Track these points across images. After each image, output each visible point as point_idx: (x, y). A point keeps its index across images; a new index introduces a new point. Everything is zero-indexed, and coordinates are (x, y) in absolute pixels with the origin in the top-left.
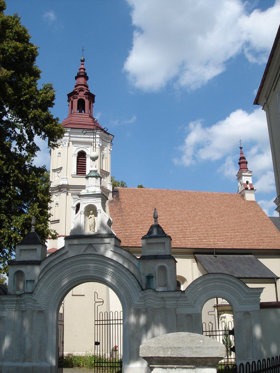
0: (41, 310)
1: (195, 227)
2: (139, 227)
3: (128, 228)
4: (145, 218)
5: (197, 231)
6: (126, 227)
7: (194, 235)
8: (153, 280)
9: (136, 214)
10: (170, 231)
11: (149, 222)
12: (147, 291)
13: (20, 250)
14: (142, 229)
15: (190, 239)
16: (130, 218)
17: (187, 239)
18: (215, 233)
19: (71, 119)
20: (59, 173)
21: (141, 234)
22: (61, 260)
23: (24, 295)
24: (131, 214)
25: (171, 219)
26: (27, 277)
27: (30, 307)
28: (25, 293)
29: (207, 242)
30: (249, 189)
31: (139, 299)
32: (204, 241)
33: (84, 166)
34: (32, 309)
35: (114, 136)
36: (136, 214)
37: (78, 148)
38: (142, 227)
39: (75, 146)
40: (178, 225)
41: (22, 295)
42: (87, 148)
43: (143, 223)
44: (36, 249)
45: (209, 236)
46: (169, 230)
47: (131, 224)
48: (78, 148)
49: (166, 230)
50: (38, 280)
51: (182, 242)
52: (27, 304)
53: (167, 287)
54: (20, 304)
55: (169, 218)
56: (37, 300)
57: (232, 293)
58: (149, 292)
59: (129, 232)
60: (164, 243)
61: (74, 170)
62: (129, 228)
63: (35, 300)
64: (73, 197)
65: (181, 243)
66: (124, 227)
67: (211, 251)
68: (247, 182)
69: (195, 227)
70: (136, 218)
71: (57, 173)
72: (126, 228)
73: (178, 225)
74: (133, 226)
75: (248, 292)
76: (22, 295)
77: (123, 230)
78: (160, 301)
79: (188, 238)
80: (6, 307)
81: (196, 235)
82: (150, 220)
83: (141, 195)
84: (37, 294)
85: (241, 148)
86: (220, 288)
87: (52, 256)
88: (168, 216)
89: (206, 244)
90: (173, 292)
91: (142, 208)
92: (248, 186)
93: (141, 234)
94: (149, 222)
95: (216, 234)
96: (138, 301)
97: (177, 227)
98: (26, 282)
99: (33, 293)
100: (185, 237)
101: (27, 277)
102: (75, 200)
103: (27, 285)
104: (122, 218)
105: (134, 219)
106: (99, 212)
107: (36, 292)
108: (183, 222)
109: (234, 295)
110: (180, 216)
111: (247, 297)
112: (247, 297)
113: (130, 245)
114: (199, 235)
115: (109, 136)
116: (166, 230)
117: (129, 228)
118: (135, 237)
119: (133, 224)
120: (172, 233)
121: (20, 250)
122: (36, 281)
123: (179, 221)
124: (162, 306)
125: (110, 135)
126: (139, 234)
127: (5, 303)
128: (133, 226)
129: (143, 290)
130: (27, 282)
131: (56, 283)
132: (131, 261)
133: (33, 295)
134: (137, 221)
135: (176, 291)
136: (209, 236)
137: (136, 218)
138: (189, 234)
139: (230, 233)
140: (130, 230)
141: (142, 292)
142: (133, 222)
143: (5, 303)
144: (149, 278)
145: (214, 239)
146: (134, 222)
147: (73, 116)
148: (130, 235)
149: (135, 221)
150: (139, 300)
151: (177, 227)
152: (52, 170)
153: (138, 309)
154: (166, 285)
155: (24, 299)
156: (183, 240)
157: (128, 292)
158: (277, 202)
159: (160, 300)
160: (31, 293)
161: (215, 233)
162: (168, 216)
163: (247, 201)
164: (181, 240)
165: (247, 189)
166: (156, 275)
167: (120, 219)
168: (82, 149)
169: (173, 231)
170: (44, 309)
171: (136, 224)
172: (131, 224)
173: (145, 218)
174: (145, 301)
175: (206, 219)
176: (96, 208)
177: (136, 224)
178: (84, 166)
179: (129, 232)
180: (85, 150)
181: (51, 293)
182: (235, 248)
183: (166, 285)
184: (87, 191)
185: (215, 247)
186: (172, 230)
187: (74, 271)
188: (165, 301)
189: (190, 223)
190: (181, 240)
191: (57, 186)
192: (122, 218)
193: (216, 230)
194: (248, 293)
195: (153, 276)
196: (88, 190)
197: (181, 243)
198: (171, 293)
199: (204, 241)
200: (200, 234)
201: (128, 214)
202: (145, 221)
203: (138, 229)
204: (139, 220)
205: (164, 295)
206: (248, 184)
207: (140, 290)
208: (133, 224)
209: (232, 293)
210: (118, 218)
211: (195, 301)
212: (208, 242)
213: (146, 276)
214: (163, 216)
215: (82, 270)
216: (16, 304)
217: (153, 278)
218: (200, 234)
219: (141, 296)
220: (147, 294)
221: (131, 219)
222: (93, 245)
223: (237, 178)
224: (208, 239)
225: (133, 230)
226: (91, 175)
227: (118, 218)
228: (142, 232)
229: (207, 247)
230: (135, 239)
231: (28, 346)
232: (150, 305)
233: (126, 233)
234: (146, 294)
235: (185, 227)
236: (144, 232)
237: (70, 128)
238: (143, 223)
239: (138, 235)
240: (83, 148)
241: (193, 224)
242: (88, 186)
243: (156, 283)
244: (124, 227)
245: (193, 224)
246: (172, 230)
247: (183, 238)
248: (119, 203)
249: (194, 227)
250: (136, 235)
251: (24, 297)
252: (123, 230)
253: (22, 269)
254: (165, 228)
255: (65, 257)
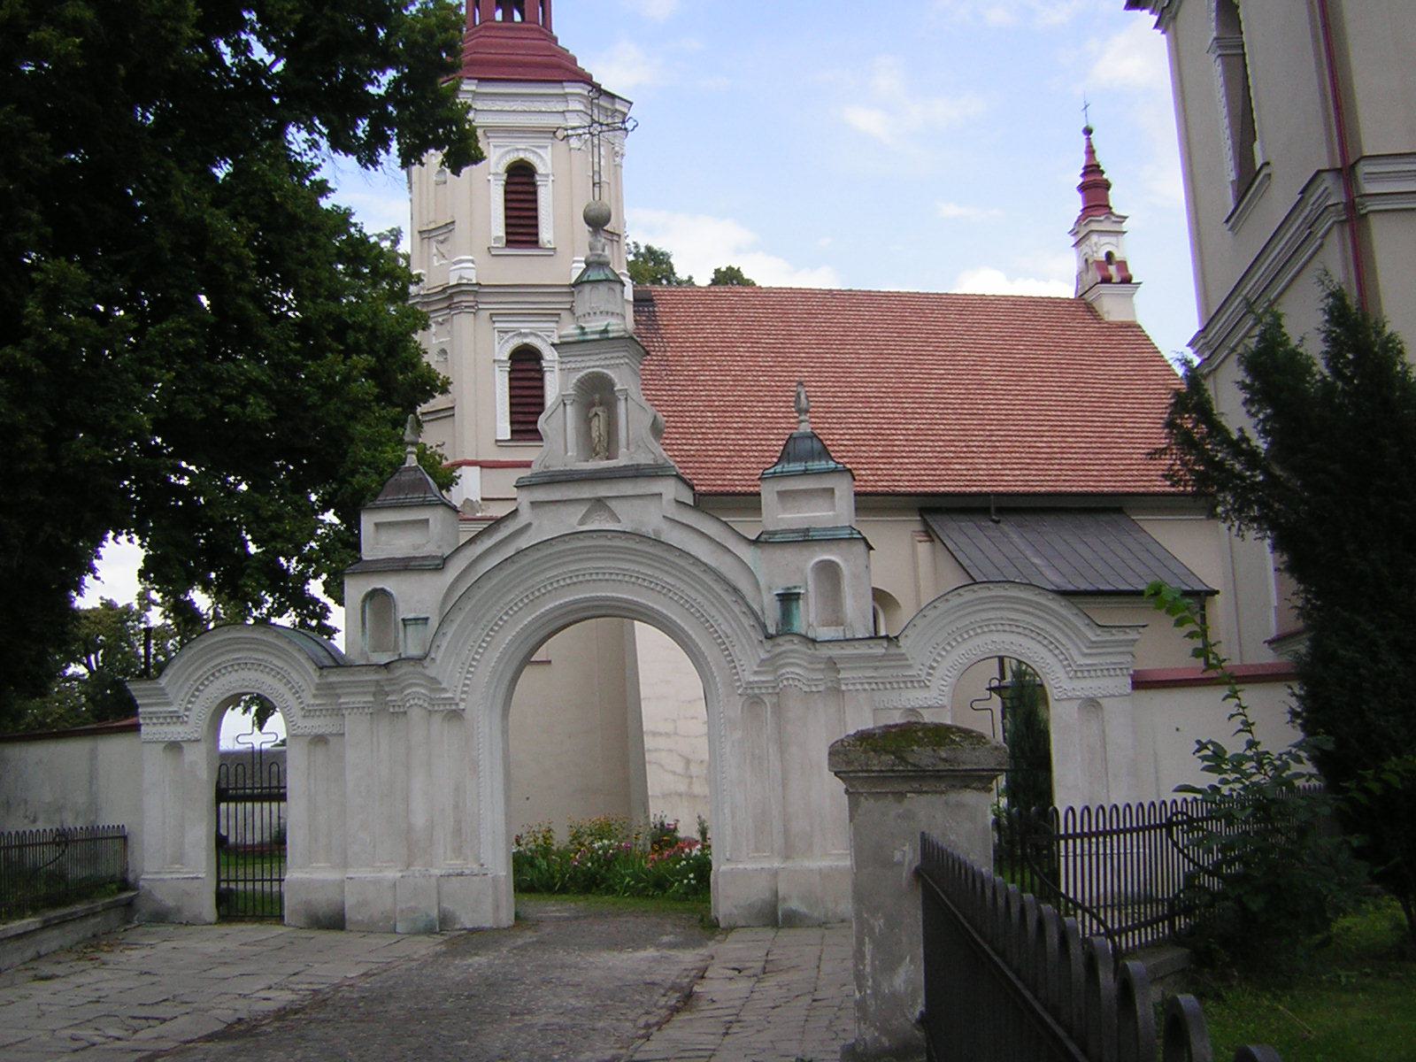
0: (454, 707)
1: (924, 421)
2: (730, 425)
3: (692, 430)
4: (751, 393)
5: (930, 432)
6: (685, 425)
7: (923, 449)
8: (798, 608)
9: (719, 378)
10: (837, 437)
11: (765, 404)
12: (780, 640)
13: (377, 525)
14: (739, 431)
15: (906, 460)
16: (697, 393)
17: (896, 460)
18: (994, 438)
19: (477, 45)
20: (442, 242)
21: (737, 448)
22: (510, 551)
23: (398, 664)
24: (702, 378)
25: (840, 394)
26: (404, 611)
27: (421, 702)
28: (400, 659)
29: (965, 472)
30: (1116, 278)
31: (317, 689)
32: (957, 467)
33: (530, 214)
34: (426, 705)
35: (631, 103)
36: (719, 378)
37: (508, 152)
38: (740, 425)
39: (495, 146)
40: (865, 415)
41: (391, 665)
42: (538, 151)
43: (745, 409)
44: (427, 521)
45: (975, 449)
46: (835, 431)
47: (704, 414)
48: (508, 152)
49: (825, 431)
50: (441, 613)
51: (879, 472)
52: (406, 692)
53: (842, 625)
54: (387, 694)
55: (833, 389)
56: (440, 678)
57: (1045, 642)
58: (785, 645)
59: (696, 442)
60: (832, 490)
61: (498, 227)
62: (698, 431)
63: (434, 680)
64: (497, 325)
65: (876, 478)
66: (679, 425)
67: (977, 503)
68: (1109, 255)
69: (924, 421)
70: (719, 393)
71: (438, 242)
72: (686, 430)
73: (865, 415)
74: (711, 420)
75: (1094, 639)
76: (395, 664)
77: (677, 436)
78: (822, 670)
79: (901, 460)
80: (343, 703)
81: (928, 449)
82: (766, 399)
83: (732, 309)
84: (438, 662)
85: (1088, 131)
86: (1007, 628)
87: (478, 542)
88: (830, 384)
89: (963, 478)
90: (863, 642)
91: (739, 359)
92: (1112, 269)
93: (737, 448)
94: (765, 404)
95: (998, 444)
96: (756, 673)
97: (862, 420)
98: (401, 624)
99: (428, 659)
100: (888, 455)
101: (404, 611)
102: (506, 337)
103: (405, 632)
104: (670, 393)
105: (714, 398)
106: (622, 398)
107: (439, 655)
108: (881, 405)
109: (1051, 647)
110: (872, 382)
111: (1091, 655)
112: (1091, 655)
113: (704, 488)
114: (938, 449)
115: (613, 104)
116: (825, 431)
117: (698, 431)
118: (718, 459)
119: (709, 414)
120: (845, 443)
121: (377, 525)
122: (434, 623)
123: (867, 401)
124: (830, 684)
125: (617, 100)
126: (731, 448)
127: (338, 691)
128: (711, 420)
129: (769, 637)
130: (405, 625)
131: (496, 624)
132: (729, 550)
133: (427, 662)
134: (722, 403)
135: (870, 638)
136: (975, 449)
137: (719, 393)
138: (905, 443)
139: (1045, 439)
140: (700, 436)
141: (768, 644)
142: (710, 406)
143: (338, 691)
144: (788, 599)
145: (991, 461)
146: (713, 409)
147: (482, 33)
148: (699, 453)
149: (717, 403)
150: (757, 669)
151: (862, 420)
152: (420, 232)
153: (756, 696)
154: (838, 622)
155: (399, 677)
156: (882, 466)
157: (725, 644)
158: (1197, 347)
159: (822, 666)
160: (419, 660)
161: (994, 438)
162: (830, 384)
163: (1107, 323)
164: (876, 466)
165: (1107, 280)
166: (807, 590)
167: (666, 398)
168: (522, 155)
169: (847, 437)
170: (462, 705)
171: (720, 414)
172: (704, 414)
173: (751, 393)
174: (775, 670)
175: (963, 391)
176: (613, 385)
177: (720, 414)
178: (530, 214)
179: (696, 442)
180: (531, 158)
181: (482, 655)
182: (1063, 489)
183: (838, 622)
184: (578, 331)
185: (995, 489)
186: (845, 431)
187: (552, 584)
188: (839, 672)
189: (906, 405)
190: (876, 466)
191: (440, 288)
192: (670, 393)
193: (998, 428)
194: (1095, 642)
195: (799, 594)
196: (582, 328)
197: (876, 478)
198: (856, 644)
199: (957, 467)
200: (941, 443)
201: (693, 380)
202: (749, 404)
203: (727, 431)
204: (731, 398)
205: (835, 651)
206: (1111, 264)
207: (762, 638)
208: (709, 414)
209: (1045, 642)
210: (659, 393)
211: (932, 668)
212: (971, 473)
213: (777, 595)
214: (814, 384)
215: (575, 580)
216: (374, 694)
217: (798, 599)
218: (941, 443)
219: (763, 655)
220: (778, 650)
221: (703, 398)
222: (608, 504)
223: (1073, 240)
224: (970, 461)
225: (710, 436)
226: (591, 279)
227: (659, 393)
228: (741, 442)
229: (968, 489)
230: (720, 465)
231: (419, 820)
232: (791, 682)
233: (686, 447)
234: (778, 650)
235: (890, 421)
236: (747, 442)
237: (476, 81)
238: (745, 409)
239: (728, 453)
240: (525, 150)
241: (919, 411)
242: (581, 313)
243: (808, 616)
244: (679, 425)
245: (919, 411)
246: (845, 431)
247: (884, 460)
248: (658, 342)
249: (919, 421)
250: (722, 454)
251: (398, 673)
252: (677, 436)
253: (389, 584)
254: (821, 425)
255: (524, 542)
